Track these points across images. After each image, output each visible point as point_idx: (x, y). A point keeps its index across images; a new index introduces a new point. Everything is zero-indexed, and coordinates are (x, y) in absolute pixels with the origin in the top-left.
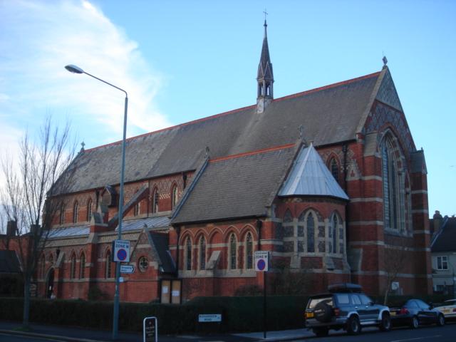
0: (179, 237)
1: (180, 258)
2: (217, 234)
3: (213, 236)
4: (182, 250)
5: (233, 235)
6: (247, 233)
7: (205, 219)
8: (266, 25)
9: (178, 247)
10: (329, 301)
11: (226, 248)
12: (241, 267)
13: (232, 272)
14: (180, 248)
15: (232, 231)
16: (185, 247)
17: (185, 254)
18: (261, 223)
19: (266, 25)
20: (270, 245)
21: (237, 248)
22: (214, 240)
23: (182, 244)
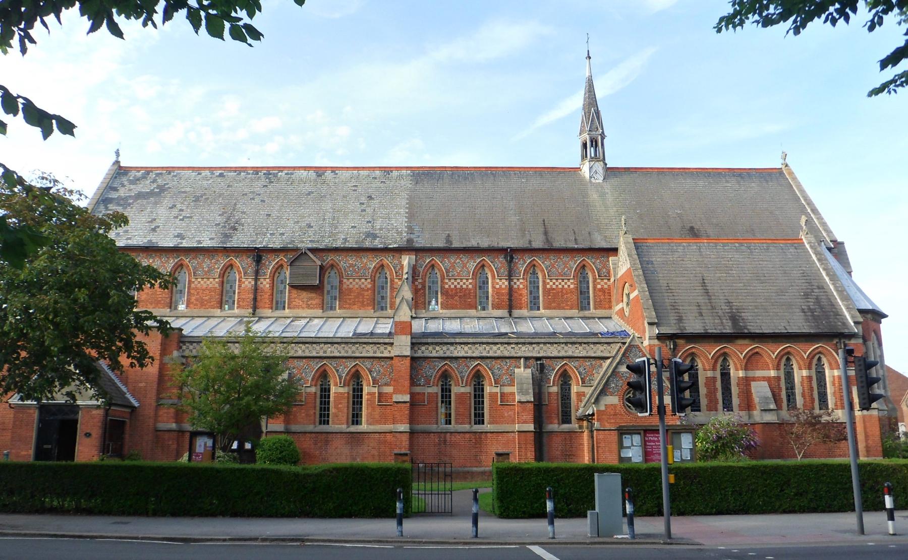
2: (758, 357)
3: (750, 357)
6: (817, 357)
11: (714, 378)
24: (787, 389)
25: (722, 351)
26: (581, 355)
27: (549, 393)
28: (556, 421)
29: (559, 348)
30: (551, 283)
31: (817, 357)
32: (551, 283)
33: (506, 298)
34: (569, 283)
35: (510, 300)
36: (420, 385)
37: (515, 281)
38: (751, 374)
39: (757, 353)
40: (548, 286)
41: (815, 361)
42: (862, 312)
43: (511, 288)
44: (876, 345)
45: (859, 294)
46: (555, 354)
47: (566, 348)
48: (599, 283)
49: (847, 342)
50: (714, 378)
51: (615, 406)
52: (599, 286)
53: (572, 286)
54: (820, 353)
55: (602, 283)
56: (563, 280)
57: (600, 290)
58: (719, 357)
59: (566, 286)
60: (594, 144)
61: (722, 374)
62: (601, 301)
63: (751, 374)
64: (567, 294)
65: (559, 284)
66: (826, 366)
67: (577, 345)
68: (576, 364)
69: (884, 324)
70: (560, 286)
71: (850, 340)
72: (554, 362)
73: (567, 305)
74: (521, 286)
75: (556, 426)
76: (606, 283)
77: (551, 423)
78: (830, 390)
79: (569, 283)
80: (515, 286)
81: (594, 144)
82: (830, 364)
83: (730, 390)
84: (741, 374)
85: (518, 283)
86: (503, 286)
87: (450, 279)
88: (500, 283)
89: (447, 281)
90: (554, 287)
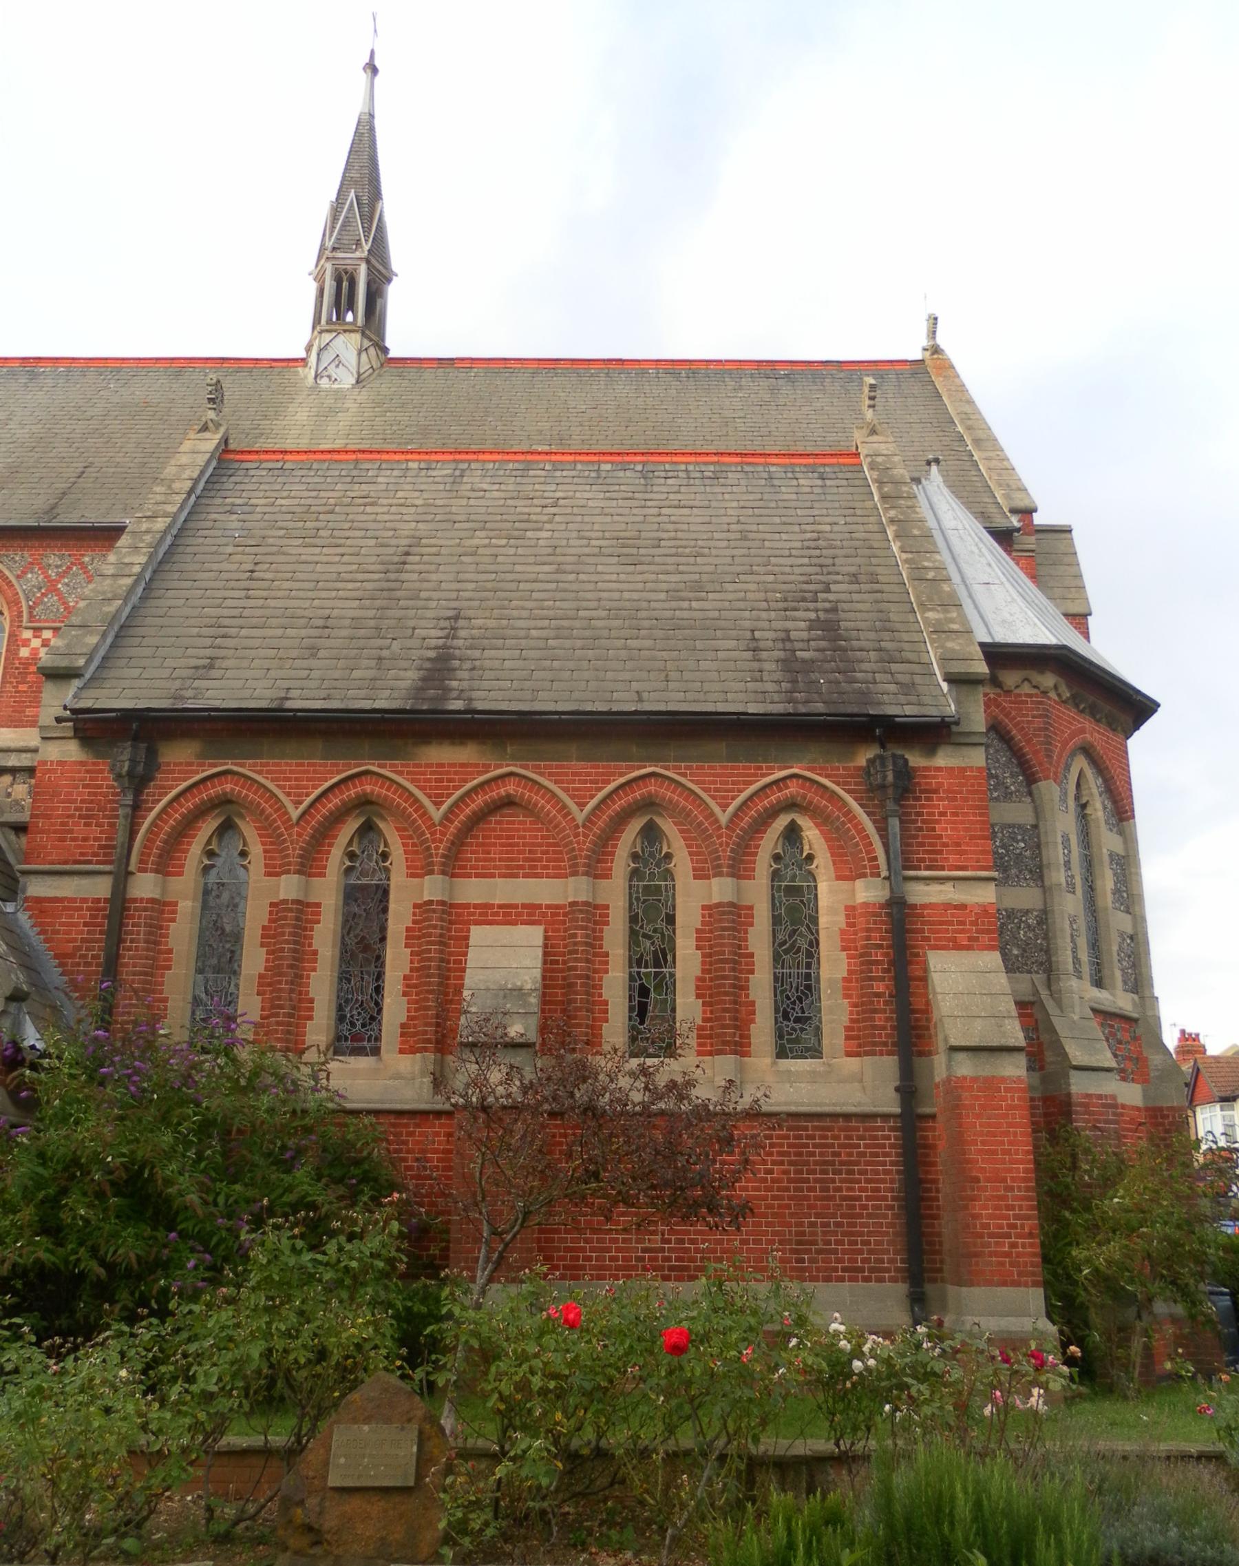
0: (137, 808)
1: (131, 960)
2: (516, 821)
3: (479, 818)
4: (162, 909)
5: (651, 833)
6: (782, 822)
7: (545, 703)
8: (372, 69)
9: (122, 877)
10: (401, 1261)
11: (595, 914)
12: (727, 1034)
13: (789, 1076)
14: (144, 886)
15: (649, 805)
16: (184, 889)
17: (182, 934)
18: (905, 775)
19: (372, 69)
20: (984, 910)
21: (254, 917)
22: (471, 855)
23: (166, 864)
24: (636, 961)
25: (352, 792)
30: (36, 643)
31: (782, 822)
32: (36, 643)
36: (1044, 917)
38: (472, 891)
39: (509, 802)
40: (24, 652)
41: (770, 841)
44: (1099, 809)
45: (969, 601)
49: (915, 760)
50: (595, 914)
54: (791, 805)
58: (337, 818)
60: (355, 288)
61: (351, 894)
63: (472, 891)
66: (823, 865)
69: (1145, 750)
71: (931, 751)
78: (833, 966)
81: (355, 288)
82: (838, 855)
83: (379, 960)
84: (432, 888)
87: (37, 630)
89: (27, 634)
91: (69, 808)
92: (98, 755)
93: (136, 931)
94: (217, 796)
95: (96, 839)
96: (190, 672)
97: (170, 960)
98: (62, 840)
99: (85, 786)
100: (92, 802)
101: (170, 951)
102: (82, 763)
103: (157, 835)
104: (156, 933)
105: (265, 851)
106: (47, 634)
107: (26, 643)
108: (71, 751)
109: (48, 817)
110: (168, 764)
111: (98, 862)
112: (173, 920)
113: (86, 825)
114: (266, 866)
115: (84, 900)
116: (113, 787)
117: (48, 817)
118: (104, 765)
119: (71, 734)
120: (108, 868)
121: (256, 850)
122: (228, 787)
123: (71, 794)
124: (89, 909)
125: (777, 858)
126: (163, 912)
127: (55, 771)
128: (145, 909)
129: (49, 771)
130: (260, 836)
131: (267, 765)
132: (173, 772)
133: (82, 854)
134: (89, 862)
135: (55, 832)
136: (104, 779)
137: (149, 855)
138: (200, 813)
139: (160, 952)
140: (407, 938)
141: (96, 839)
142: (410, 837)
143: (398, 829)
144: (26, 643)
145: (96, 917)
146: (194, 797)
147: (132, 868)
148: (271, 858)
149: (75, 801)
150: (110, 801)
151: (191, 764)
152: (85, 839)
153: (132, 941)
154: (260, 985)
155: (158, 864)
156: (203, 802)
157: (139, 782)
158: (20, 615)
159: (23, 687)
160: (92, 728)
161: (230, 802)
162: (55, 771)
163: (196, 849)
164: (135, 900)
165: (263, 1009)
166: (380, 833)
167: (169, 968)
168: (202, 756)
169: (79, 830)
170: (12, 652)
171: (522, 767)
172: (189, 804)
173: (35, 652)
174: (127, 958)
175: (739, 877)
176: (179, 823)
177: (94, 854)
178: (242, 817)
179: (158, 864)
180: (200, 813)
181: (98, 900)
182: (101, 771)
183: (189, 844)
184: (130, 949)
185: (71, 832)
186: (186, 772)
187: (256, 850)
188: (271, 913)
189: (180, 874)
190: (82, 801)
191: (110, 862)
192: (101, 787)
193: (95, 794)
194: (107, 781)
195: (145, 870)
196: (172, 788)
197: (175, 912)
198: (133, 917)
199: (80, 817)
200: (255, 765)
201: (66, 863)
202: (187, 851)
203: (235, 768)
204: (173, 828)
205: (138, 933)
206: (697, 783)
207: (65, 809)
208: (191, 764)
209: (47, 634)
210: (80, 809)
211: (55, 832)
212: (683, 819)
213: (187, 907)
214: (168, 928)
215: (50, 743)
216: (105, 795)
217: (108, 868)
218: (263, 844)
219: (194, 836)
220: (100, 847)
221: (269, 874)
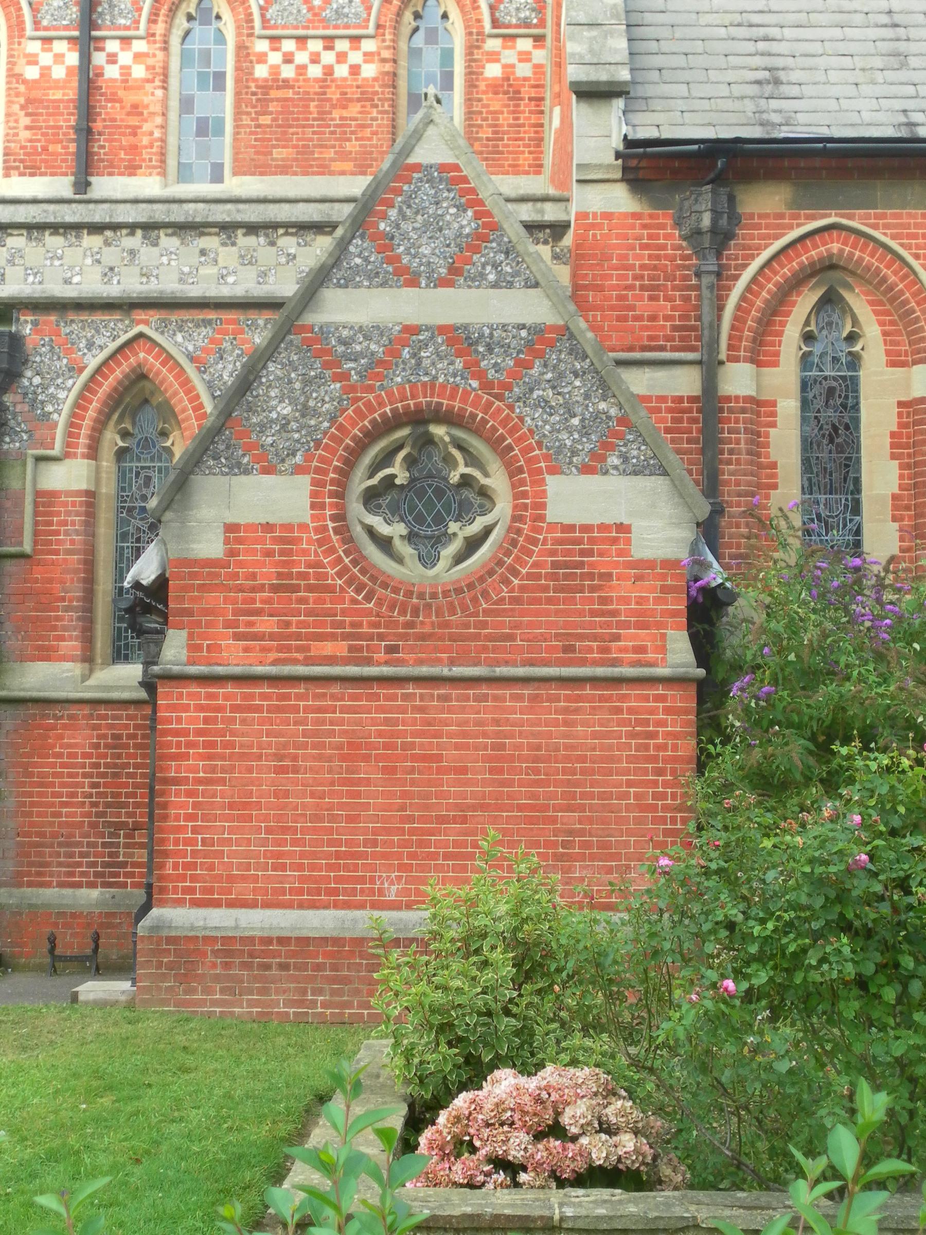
4: (760, 408)
9: (710, 369)
16: (782, 383)
17: (785, 441)
23: (761, 354)
26: (225, 292)
27: (46, 500)
28: (71, 645)
29: (111, 256)
30: (275, 58)
32: (275, 58)
33: (68, 121)
34: (355, 57)
35: (86, 133)
37: (112, 46)
40: (261, 72)
42: (660, 1182)
43: (88, 80)
46: (89, 283)
47: (148, 254)
48: (494, 57)
51: (283, 536)
52: (493, 71)
53: (369, 71)
55: (509, 57)
56: (329, 42)
57: (495, 87)
59: (342, 71)
62: (497, 136)
64: (344, 102)
65: (309, 61)
67: (211, 242)
68: (202, 337)
70: (315, 71)
72: (74, 327)
73: (343, 156)
74: (139, 72)
75: (72, 669)
76: (525, 57)
77: (46, 654)
79: (355, 57)
80: (112, 72)
85: (125, 58)
86: (59, 73)
88: (46, 59)
90: (288, 72)
91: (625, 277)
92: (657, 204)
93: (735, 440)
94: (821, 259)
95: (667, 318)
96: (753, 90)
97: (774, 476)
98: (624, 319)
99: (644, 247)
100: (655, 268)
101: (774, 465)
102: (635, 216)
103: (748, 312)
104: (758, 443)
105: (885, 334)
106: (342, 45)
107: (262, 58)
108: (619, 199)
109: (600, 289)
110: (752, 216)
111: (674, 349)
112: (773, 425)
113: (651, 298)
114: (888, 353)
115: (662, 399)
116: (680, 248)
117: (600, 289)
118: (666, 218)
119: (619, 175)
120: (690, 356)
121: (872, 331)
122: (835, 247)
123: (626, 257)
124: (670, 410)
125: (808, 338)
126: (758, 414)
127: (599, 226)
128: (743, 410)
129: (593, 226)
130: (876, 313)
131: (884, 216)
132: (758, 227)
133: (651, 338)
134: (662, 349)
135: (612, 308)
136: (666, 237)
137: (740, 339)
138: (796, 283)
139: (760, 466)
140: (893, 446)
141: (667, 318)
142: (888, 313)
143: (871, 303)
144: (262, 58)
145: (680, 421)
146: (791, 260)
147: (723, 356)
148: (893, 343)
149: (632, 267)
150: (679, 267)
151: (781, 216)
152: (653, 318)
153: (731, 452)
154: (895, 507)
155: (752, 350)
156: (802, 268)
157: (721, 238)
158: (249, 19)
159: (265, 120)
160: (652, 166)
161: (833, 267)
162: (599, 226)
163: (792, 331)
164: (728, 399)
165: (902, 539)
166: (846, 309)
167: (775, 487)
168: (796, 204)
169: (644, 306)
170: (13, 76)
171: (842, 216)
172: (785, 271)
173: (509, 68)
174: (727, 472)
175: (759, 364)
176: (773, 295)
177: (668, 339)
178: (850, 288)
179: (752, 350)
180: (796, 283)
181: (680, 399)
182: (663, 227)
183: (783, 324)
184: (729, 462)
185: (632, 308)
186: (778, 226)
187: (872, 331)
188: (900, 415)
189: (776, 364)
190: (642, 267)
191: (693, 349)
192: (664, 247)
193: (658, 257)
194: (671, 238)
195: (736, 360)
196: (760, 248)
197: (774, 414)
198: (729, 420)
199: (642, 288)
200: (868, 217)
201: (631, 349)
202: (780, 334)
203: (844, 221)
204: (766, 302)
205: (738, 442)
206: (893, 237)
207: (619, 278)
208: (781, 216)
209: (289, 46)
210: (642, 277)
211: (612, 308)
212: (877, 285)
213: (789, 407)
214: (767, 435)
215: (589, 188)
216: (672, 259)
217: (690, 356)
218: (881, 323)
219: (788, 314)
220: (675, 328)
221: (892, 364)
